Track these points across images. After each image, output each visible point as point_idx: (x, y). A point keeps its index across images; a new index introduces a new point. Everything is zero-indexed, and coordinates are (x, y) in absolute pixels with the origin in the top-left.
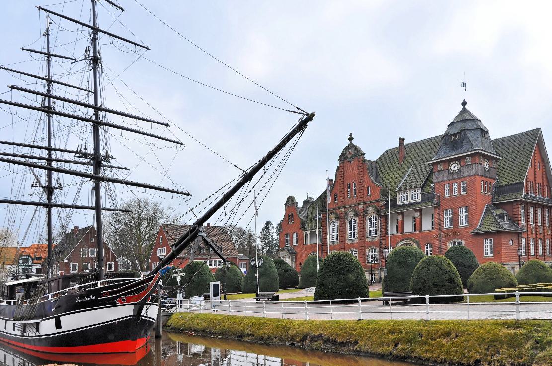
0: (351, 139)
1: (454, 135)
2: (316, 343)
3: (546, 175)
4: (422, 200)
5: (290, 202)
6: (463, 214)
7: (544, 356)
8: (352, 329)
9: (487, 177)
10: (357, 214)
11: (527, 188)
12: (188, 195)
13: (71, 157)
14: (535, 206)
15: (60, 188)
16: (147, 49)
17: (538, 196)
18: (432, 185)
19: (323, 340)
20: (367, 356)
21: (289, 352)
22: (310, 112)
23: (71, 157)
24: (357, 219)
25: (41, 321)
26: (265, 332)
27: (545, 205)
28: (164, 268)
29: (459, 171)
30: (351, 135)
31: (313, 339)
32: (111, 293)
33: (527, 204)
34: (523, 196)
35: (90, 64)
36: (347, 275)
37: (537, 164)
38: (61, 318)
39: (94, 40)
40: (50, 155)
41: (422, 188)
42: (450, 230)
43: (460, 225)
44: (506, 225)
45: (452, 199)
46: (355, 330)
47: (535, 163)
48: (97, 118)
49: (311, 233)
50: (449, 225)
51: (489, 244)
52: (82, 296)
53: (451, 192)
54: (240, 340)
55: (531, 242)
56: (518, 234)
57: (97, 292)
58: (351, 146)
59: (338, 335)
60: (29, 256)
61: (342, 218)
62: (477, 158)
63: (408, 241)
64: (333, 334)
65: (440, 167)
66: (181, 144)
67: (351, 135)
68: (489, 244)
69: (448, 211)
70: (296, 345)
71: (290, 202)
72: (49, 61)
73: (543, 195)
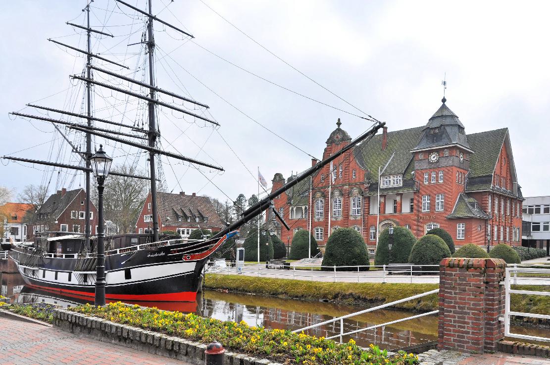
0: (339, 124)
2: (347, 300)
3: (510, 170)
4: (403, 186)
5: (278, 178)
6: (440, 200)
7: (537, 310)
8: (379, 289)
9: (461, 168)
10: (342, 195)
12: (222, 170)
13: (128, 131)
14: (500, 196)
16: (192, 37)
17: (496, 186)
18: (413, 173)
23: (128, 131)
24: (342, 199)
26: (300, 290)
27: (496, 193)
28: (231, 232)
29: (438, 162)
30: (339, 120)
31: (344, 297)
32: (178, 251)
33: (493, 194)
34: (491, 188)
36: (353, 248)
37: (503, 160)
39: (150, 27)
40: (89, 123)
41: (404, 175)
42: (426, 214)
44: (476, 212)
48: (152, 97)
49: (297, 208)
50: (425, 210)
52: (154, 252)
53: (429, 180)
56: (486, 221)
57: (167, 250)
58: (339, 130)
59: (367, 294)
60: (5, 214)
61: (346, 195)
63: (390, 222)
65: (421, 157)
66: (217, 124)
67: (339, 120)
68: (461, 227)
71: (278, 178)
72: (89, 36)
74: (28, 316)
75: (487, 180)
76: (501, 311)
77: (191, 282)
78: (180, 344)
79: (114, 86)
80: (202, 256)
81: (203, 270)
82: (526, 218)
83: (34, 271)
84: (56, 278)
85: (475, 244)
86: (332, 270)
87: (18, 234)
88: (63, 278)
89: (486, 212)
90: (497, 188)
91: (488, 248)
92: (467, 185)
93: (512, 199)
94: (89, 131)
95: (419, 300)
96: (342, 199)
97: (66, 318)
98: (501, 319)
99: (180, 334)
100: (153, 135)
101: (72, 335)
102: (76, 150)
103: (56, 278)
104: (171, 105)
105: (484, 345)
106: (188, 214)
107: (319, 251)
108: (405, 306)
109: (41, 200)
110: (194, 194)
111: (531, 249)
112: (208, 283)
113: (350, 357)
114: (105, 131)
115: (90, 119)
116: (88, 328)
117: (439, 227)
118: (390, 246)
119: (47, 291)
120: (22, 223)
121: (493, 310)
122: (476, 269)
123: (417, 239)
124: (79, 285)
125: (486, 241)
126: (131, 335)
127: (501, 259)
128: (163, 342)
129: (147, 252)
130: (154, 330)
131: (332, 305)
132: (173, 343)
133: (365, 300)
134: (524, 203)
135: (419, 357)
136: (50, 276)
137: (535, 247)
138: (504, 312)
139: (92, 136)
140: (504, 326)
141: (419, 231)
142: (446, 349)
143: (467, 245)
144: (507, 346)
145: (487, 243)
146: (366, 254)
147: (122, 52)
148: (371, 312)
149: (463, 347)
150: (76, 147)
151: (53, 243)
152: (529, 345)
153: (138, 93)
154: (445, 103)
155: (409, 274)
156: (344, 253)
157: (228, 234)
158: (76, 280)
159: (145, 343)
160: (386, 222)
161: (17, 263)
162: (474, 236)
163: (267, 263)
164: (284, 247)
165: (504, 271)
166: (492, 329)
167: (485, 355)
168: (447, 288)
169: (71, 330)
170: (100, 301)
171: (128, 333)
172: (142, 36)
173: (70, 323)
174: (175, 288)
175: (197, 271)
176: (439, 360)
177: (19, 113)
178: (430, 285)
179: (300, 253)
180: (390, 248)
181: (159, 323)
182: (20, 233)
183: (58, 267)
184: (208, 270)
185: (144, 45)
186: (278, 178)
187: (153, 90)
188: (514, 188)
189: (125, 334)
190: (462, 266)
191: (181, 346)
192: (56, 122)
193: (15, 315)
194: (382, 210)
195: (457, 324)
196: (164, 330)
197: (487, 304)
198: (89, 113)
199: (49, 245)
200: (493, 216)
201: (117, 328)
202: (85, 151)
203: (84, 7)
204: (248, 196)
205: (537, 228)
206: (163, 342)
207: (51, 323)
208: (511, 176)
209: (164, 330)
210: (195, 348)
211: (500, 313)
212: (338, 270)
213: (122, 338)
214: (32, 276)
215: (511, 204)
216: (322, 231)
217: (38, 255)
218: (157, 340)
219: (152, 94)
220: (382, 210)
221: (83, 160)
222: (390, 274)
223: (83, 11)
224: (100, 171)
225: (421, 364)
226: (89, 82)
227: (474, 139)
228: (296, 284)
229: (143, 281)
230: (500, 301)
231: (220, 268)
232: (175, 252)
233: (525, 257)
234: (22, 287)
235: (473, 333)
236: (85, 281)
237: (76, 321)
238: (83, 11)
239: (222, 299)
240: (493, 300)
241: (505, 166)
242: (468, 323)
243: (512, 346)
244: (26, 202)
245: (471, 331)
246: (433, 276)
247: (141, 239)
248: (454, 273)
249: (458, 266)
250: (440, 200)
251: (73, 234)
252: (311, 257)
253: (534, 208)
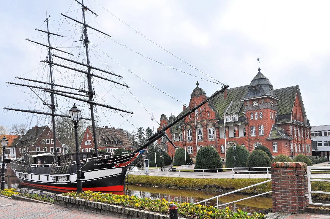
0: (198, 84)
1: (255, 86)
3: (302, 110)
4: (239, 121)
5: (163, 118)
6: (261, 128)
9: (273, 110)
10: (202, 126)
11: (293, 116)
12: (132, 113)
13: (77, 92)
14: (300, 127)
15: (57, 106)
16: (110, 36)
18: (244, 113)
19: (216, 187)
20: (241, 194)
21: (197, 194)
22: (227, 85)
23: (77, 92)
24: (202, 129)
25: (71, 175)
27: (295, 124)
29: (258, 106)
30: (197, 82)
31: (210, 187)
33: (293, 125)
35: (84, 44)
37: (297, 104)
38: (85, 173)
39: (85, 31)
40: (52, 87)
41: (238, 114)
42: (253, 137)
43: (259, 135)
44: (283, 136)
45: (255, 121)
46: (233, 183)
47: (296, 103)
49: (176, 135)
50: (253, 135)
51: (275, 145)
52: (97, 163)
54: (168, 188)
55: (299, 146)
56: (289, 141)
57: (105, 161)
58: (198, 89)
59: (224, 185)
61: (205, 127)
62: (268, 99)
64: (221, 184)
67: (197, 82)
68: (275, 145)
69: (261, 126)
70: (202, 190)
71: (163, 118)
72: (49, 37)
73: (300, 120)
74: (37, 200)
75: (288, 116)
76: (306, 190)
77: (120, 180)
78: (133, 211)
79: (68, 66)
80: (125, 164)
81: (126, 173)
82: (313, 139)
83: (25, 175)
84: (39, 179)
85: (284, 155)
86: (202, 171)
87: (9, 154)
88: (43, 179)
89: (289, 135)
90: (295, 121)
91: (292, 157)
92: (277, 119)
93: (304, 128)
94: (52, 92)
95: (255, 188)
96: (202, 129)
97: (62, 200)
98: (306, 195)
99: (131, 206)
100: (91, 94)
101: (66, 209)
102: (46, 103)
103: (39, 179)
104: (101, 76)
105: (298, 209)
106: (111, 140)
107: (190, 161)
108: (247, 191)
109: (22, 133)
110: (113, 128)
111: (318, 157)
112: (130, 180)
113: (228, 215)
114: (64, 92)
115: (52, 85)
116: (77, 205)
117: (262, 145)
118: (234, 157)
119: (35, 187)
120: (12, 147)
121: (302, 190)
122: (291, 168)
123: (250, 153)
124: (53, 183)
125: (291, 153)
126: (103, 208)
127: (304, 163)
128: (123, 211)
129: (93, 162)
130: (116, 204)
131: (204, 192)
132: (129, 211)
133: (223, 188)
134: (312, 130)
135: (265, 216)
136: (35, 178)
137: (320, 156)
138: (308, 191)
139: (54, 94)
140: (308, 199)
141: (250, 148)
142: (278, 211)
143: (280, 155)
144: (311, 209)
145: (292, 155)
146: (220, 162)
147: (68, 44)
148: (227, 195)
149: (287, 210)
150: (45, 102)
151: (35, 158)
152: (323, 208)
153: (81, 70)
154: (260, 71)
155: (248, 173)
156: (207, 161)
157: (140, 151)
158: (51, 180)
159: (112, 212)
160: (230, 142)
161: (14, 171)
162: (283, 150)
163: (162, 168)
164: (170, 158)
165: (306, 169)
166: (302, 200)
167: (299, 214)
168: (276, 179)
169: (66, 206)
170: (80, 191)
171: (101, 206)
172: (81, 36)
173: (65, 202)
174: (111, 183)
175: (123, 173)
176: (276, 217)
177: (12, 82)
178: (261, 179)
179: (180, 162)
180: (235, 158)
181: (119, 201)
182: (11, 152)
183: (40, 172)
184: (128, 172)
185: (83, 42)
186: (163, 117)
187: (90, 68)
188: (305, 121)
189: (100, 207)
190: (283, 167)
191: (134, 213)
192: (31, 87)
193: (30, 199)
194: (228, 135)
195: (283, 198)
196: (121, 204)
197: (298, 187)
198: (52, 82)
199: (33, 160)
200: (294, 138)
201: (94, 204)
202: (51, 104)
203: (45, 20)
204: (145, 129)
205: (320, 144)
206: (123, 211)
207: (53, 203)
208: (303, 114)
209: (121, 204)
210: (142, 213)
211: (306, 191)
212: (205, 171)
213: (97, 209)
214: (24, 178)
215: (304, 131)
216: (192, 149)
217: (26, 166)
218: (119, 210)
219: (89, 70)
220: (228, 135)
221: (50, 109)
222: (236, 173)
223: (44, 22)
224: (76, 118)
225: (266, 218)
226: (51, 63)
227: (277, 92)
228: (181, 180)
229: (91, 179)
230: (305, 185)
231: (135, 171)
232: (110, 162)
233: (315, 162)
234: (19, 184)
235: (292, 203)
236: (57, 180)
237: (68, 201)
238: (44, 22)
239: (137, 190)
240: (302, 185)
241: (299, 107)
242: (289, 197)
243: (314, 209)
244: (13, 134)
245: (291, 202)
246: (261, 174)
247: (89, 155)
248: (279, 170)
249: (281, 167)
250: (261, 128)
251: (46, 153)
252: (187, 164)
253: (318, 132)
